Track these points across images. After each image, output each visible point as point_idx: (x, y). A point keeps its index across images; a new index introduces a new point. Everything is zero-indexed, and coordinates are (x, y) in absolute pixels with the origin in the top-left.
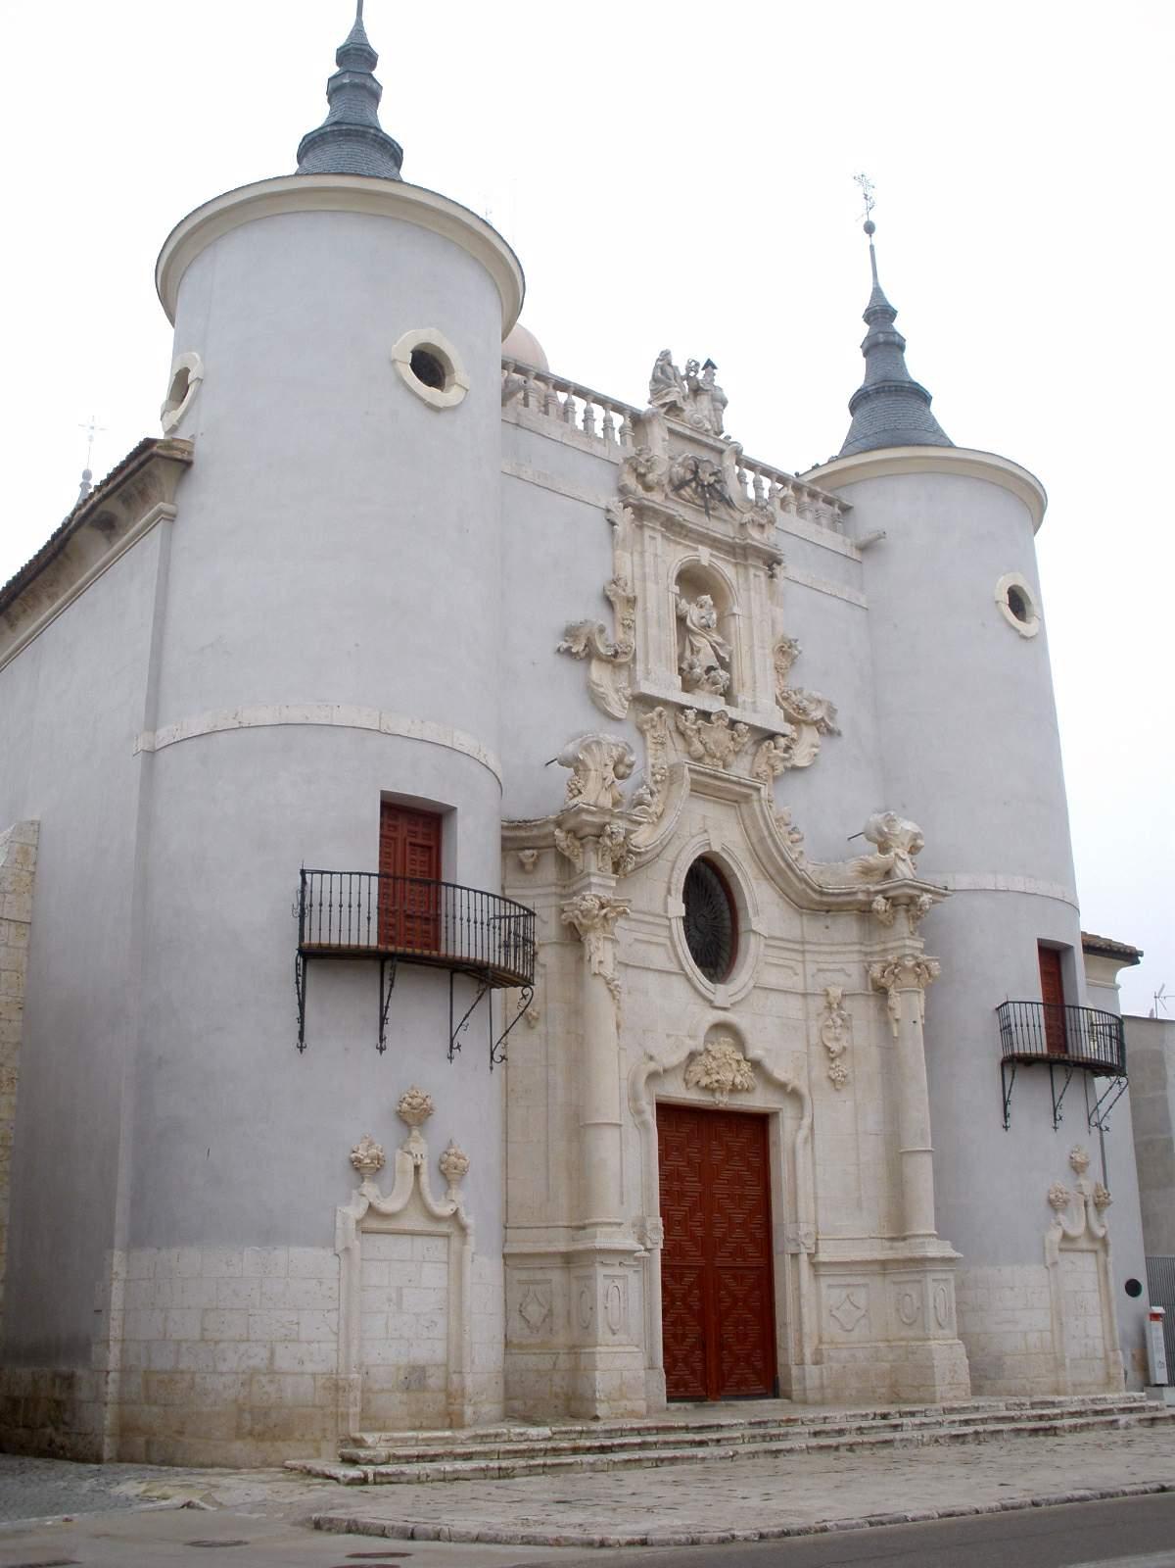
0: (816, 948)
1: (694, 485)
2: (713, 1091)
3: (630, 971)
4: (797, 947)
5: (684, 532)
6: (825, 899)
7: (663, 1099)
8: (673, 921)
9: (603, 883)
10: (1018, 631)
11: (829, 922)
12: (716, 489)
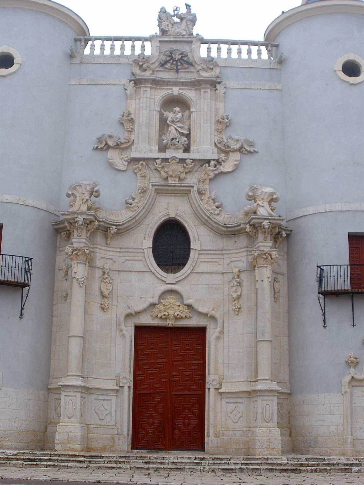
0: (228, 252)
1: (171, 61)
2: (166, 318)
3: (122, 273)
4: (220, 252)
5: (166, 83)
6: (229, 229)
7: (138, 324)
8: (146, 251)
9: (78, 241)
10: (348, 82)
11: (236, 239)
12: (184, 61)
